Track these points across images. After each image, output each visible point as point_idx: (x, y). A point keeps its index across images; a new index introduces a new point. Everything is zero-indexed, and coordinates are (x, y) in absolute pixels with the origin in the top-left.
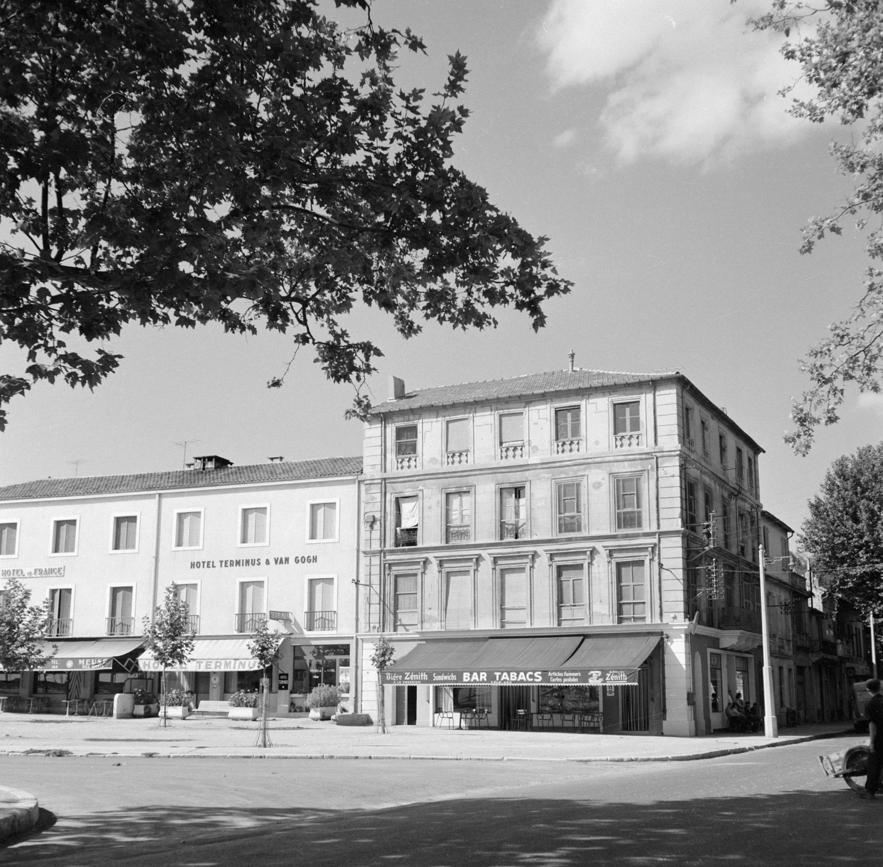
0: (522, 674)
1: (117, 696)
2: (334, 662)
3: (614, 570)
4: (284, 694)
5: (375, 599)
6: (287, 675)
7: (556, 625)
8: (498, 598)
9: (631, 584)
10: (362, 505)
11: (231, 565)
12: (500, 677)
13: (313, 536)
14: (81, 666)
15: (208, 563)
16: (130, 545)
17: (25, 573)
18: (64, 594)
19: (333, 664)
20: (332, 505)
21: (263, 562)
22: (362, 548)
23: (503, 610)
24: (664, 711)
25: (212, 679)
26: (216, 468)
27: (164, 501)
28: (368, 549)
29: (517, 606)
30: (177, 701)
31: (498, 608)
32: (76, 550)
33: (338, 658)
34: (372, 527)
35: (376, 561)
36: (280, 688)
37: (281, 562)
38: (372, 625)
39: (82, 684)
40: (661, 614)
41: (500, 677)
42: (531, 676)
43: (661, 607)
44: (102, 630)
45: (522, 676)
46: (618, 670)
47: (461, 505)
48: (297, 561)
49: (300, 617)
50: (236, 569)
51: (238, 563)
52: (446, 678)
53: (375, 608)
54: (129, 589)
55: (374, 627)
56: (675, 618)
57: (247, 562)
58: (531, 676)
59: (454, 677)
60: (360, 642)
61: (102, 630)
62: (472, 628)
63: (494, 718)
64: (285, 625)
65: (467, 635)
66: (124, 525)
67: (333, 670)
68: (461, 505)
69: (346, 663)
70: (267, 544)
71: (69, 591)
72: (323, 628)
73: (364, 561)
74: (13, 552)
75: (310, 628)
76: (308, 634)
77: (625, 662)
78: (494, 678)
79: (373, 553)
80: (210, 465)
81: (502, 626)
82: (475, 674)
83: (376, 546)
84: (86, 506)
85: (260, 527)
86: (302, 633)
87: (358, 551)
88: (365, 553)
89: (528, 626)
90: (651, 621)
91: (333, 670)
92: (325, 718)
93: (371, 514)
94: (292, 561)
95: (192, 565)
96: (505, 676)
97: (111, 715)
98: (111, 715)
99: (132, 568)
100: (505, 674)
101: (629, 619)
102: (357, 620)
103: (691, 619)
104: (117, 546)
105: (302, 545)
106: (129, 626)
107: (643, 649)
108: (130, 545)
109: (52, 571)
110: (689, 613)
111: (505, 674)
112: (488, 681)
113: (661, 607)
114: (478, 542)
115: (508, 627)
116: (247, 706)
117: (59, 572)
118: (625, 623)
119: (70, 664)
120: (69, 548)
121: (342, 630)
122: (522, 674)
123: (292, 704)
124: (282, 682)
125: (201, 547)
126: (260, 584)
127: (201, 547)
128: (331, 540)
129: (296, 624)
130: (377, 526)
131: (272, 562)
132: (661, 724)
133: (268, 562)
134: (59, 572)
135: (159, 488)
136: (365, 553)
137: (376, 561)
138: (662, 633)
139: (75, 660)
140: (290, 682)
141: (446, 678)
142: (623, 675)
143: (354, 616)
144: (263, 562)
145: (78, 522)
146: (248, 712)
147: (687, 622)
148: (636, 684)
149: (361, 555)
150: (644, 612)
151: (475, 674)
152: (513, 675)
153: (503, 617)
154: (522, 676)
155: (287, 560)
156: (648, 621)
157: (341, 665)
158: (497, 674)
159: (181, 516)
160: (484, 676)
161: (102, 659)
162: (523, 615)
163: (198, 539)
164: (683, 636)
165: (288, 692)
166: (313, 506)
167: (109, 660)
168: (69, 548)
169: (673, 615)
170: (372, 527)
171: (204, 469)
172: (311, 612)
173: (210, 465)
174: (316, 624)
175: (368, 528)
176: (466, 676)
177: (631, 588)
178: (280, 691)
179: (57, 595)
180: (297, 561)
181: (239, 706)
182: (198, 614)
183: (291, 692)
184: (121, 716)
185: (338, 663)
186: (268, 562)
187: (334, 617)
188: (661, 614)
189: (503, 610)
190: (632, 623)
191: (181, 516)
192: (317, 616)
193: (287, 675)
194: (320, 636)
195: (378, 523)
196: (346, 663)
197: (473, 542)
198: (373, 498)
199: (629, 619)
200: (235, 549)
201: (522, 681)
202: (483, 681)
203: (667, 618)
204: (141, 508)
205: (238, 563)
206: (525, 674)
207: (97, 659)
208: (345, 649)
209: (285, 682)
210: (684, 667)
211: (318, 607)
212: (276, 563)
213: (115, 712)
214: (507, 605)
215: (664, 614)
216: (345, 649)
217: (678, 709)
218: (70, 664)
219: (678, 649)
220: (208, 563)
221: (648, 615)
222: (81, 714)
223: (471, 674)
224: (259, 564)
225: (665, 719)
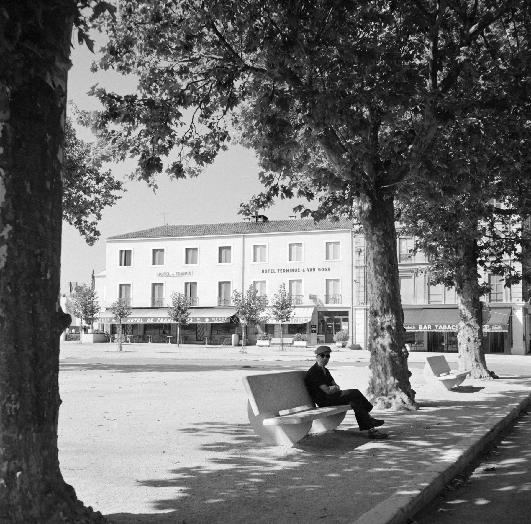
0: (449, 326)
1: (233, 335)
2: (340, 319)
3: (487, 277)
4: (314, 335)
5: (362, 289)
6: (315, 325)
7: (427, 304)
8: (427, 290)
9: (496, 284)
10: (354, 243)
11: (284, 271)
12: (438, 327)
13: (327, 258)
14: (213, 321)
15: (272, 270)
16: (228, 260)
17: (171, 274)
18: (193, 285)
19: (339, 320)
20: (338, 243)
21: (301, 270)
22: (354, 264)
23: (429, 295)
24: (512, 344)
25: (276, 328)
26: (263, 221)
27: (246, 239)
28: (358, 265)
29: (436, 293)
30: (266, 338)
31: (427, 294)
32: (198, 262)
33: (341, 318)
34: (359, 254)
35: (362, 270)
36: (312, 332)
37: (311, 270)
38: (360, 302)
39: (205, 329)
40: (511, 298)
41: (438, 327)
42: (454, 327)
43: (511, 295)
44: (215, 304)
45: (449, 327)
46: (498, 325)
47: (407, 244)
48: (319, 270)
49: (322, 298)
50: (286, 273)
51: (288, 270)
52: (410, 328)
53: (362, 294)
54: (129, 285)
55: (362, 303)
56: (518, 300)
57: (293, 270)
58: (454, 327)
59: (414, 328)
60: (354, 310)
61: (215, 304)
62: (414, 304)
63: (426, 346)
64: (314, 301)
65: (411, 307)
66: (157, 254)
67: (339, 323)
68: (407, 244)
69: (346, 320)
70: (303, 261)
71: (196, 283)
72: (334, 303)
73: (355, 270)
74: (163, 264)
75: (327, 303)
76: (326, 306)
77: (500, 322)
78: (435, 328)
79: (361, 267)
80: (260, 220)
81: (429, 303)
82: (425, 326)
83: (362, 263)
84: (202, 241)
85: (298, 253)
86: (323, 305)
87: (352, 266)
88: (356, 267)
89: (443, 303)
90: (506, 301)
91: (339, 323)
92: (344, 346)
93: (359, 248)
94: (317, 270)
95: (263, 271)
96: (441, 327)
97: (231, 344)
98: (231, 344)
99: (230, 272)
100: (441, 326)
101: (494, 300)
102: (352, 299)
103: (526, 301)
104: (220, 261)
105: (322, 262)
106: (162, 303)
107: (505, 314)
108: (228, 260)
109: (185, 273)
110: (525, 298)
111: (441, 326)
112: (416, 329)
113: (511, 295)
114: (416, 262)
115: (432, 303)
116: (303, 340)
117: (190, 274)
118: (492, 303)
119: (207, 320)
120: (194, 261)
121: (343, 304)
122: (449, 326)
123: (318, 340)
124: (313, 329)
125: (267, 263)
126: (300, 281)
127: (267, 263)
128: (338, 260)
129: (320, 300)
130: (362, 254)
131: (306, 270)
132: (510, 350)
133: (304, 270)
134: (190, 274)
135: (242, 233)
136: (356, 267)
137: (362, 270)
138: (511, 308)
139: (210, 318)
140: (317, 329)
141: (410, 328)
142: (500, 327)
143: (351, 297)
144: (301, 270)
145: (198, 249)
146: (304, 343)
147: (524, 302)
148: (507, 331)
149: (354, 267)
150: (502, 297)
151: (425, 326)
152: (445, 327)
153: (429, 299)
154: (449, 327)
155: (314, 269)
156: (504, 302)
157: (343, 321)
158: (437, 326)
159: (255, 247)
160: (430, 327)
161: (224, 318)
162: (441, 298)
163: (197, 261)
164: (522, 309)
165: (316, 333)
166: (290, 245)
167: (228, 318)
168: (194, 261)
169: (517, 299)
170: (359, 254)
171: (257, 222)
172: (327, 296)
173: (260, 220)
174: (330, 301)
175: (358, 255)
176: (420, 327)
177: (495, 286)
178: (312, 334)
179: (189, 286)
180: (319, 270)
181: (299, 340)
182: (303, 294)
183: (318, 334)
184: (235, 346)
185: (341, 320)
186: (304, 270)
187: (340, 298)
188: (511, 298)
189: (429, 295)
190: (496, 302)
191: (255, 247)
192: (330, 297)
193: (315, 325)
194: (331, 307)
195: (363, 252)
196: (346, 320)
197: (414, 263)
198: (360, 240)
199: (494, 300)
200: (286, 264)
201: (449, 330)
202: (429, 329)
203: (514, 301)
204: (234, 243)
205: (288, 270)
206: (451, 326)
207: (222, 318)
208: (346, 313)
209: (315, 329)
210: (522, 323)
211: (331, 293)
212: (308, 271)
213: (233, 343)
214: (431, 293)
215: (512, 298)
216: (346, 313)
217: (519, 343)
218: (207, 320)
219: (519, 315)
220: (272, 270)
221: (504, 298)
222: (136, 342)
223: (423, 326)
224: (299, 271)
225: (512, 347)
